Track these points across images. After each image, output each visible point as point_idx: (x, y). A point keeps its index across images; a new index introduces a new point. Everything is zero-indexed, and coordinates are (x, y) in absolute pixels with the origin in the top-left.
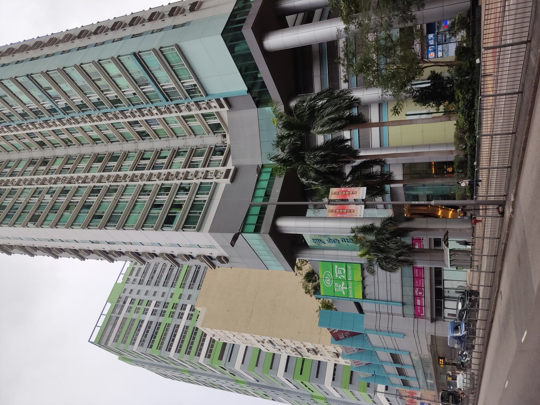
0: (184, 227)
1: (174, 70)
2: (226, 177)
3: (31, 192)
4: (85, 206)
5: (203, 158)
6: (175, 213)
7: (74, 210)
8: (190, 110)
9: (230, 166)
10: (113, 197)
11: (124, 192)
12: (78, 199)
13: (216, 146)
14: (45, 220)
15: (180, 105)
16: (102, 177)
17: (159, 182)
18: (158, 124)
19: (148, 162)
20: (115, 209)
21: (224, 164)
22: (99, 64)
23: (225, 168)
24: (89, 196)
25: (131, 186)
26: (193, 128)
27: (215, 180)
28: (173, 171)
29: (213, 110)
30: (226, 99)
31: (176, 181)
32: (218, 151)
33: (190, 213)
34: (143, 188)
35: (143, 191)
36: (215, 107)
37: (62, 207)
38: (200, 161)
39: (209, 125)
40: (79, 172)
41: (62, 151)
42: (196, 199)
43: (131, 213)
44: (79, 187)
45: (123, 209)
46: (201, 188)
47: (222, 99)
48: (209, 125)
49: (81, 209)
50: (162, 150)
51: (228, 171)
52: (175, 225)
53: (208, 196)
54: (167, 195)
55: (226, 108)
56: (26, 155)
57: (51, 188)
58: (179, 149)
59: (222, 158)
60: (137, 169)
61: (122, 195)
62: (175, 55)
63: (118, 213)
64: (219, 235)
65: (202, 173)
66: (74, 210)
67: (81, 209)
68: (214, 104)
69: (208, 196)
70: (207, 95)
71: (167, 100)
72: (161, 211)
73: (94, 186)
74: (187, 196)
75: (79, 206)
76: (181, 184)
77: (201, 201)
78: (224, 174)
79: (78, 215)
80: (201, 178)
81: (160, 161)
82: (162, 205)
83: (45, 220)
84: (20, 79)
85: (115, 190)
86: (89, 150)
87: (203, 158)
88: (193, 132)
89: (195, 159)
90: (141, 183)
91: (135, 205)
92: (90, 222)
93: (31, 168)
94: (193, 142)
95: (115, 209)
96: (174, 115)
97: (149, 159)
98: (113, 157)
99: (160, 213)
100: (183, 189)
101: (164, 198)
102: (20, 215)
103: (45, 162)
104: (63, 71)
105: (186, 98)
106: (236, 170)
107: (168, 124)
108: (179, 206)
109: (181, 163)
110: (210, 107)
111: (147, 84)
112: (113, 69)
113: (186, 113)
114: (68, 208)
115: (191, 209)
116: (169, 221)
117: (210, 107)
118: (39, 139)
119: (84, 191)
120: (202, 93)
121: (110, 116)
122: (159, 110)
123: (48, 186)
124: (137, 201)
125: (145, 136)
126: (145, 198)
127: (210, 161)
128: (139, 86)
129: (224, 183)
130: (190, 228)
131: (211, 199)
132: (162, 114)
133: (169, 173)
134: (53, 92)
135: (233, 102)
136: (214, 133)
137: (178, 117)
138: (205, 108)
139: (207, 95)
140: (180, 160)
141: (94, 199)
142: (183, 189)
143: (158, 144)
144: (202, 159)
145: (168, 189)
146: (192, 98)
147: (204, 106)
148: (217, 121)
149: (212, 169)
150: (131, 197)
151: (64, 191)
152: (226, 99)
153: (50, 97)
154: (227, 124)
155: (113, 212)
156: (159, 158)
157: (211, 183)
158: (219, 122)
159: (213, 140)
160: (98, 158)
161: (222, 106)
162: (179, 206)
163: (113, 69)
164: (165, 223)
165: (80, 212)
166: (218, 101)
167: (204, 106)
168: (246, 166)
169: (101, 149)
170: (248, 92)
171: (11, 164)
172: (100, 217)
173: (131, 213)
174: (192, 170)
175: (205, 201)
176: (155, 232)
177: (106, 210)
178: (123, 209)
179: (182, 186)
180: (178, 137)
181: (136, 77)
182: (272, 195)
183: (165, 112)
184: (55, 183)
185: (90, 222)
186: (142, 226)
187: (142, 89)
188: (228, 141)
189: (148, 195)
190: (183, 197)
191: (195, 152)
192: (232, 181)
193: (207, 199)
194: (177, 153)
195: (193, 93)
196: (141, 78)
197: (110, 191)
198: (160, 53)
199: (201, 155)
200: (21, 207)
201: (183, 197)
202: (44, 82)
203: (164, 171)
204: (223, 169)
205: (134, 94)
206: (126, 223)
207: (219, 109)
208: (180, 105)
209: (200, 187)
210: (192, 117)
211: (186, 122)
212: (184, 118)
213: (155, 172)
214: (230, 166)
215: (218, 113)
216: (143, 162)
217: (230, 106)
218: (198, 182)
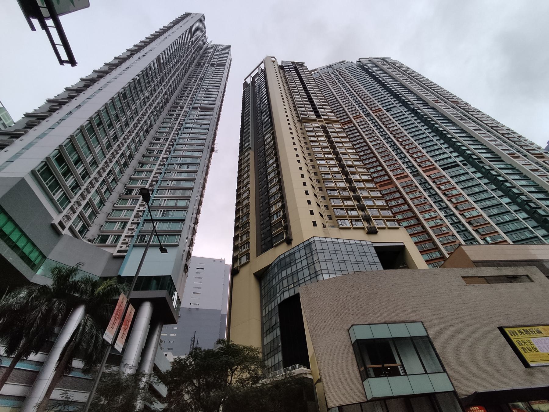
0: (46, 164)
1: (163, 235)
2: (60, 223)
3: (139, 110)
4: (111, 125)
5: (87, 217)
6: (63, 168)
7: (113, 118)
8: (129, 229)
9: (66, 232)
10: (104, 143)
11: (103, 152)
12: (118, 126)
13: (88, 230)
14: (120, 99)
15: (136, 225)
16: (120, 149)
17: (92, 176)
18: (131, 204)
19: (110, 180)
20: (96, 137)
21: (71, 229)
22: (188, 199)
23: (67, 227)
24: (115, 133)
25: (103, 159)
26: (113, 224)
27: (65, 212)
28: (93, 191)
29: (119, 244)
30: (123, 257)
31: (83, 188)
32: (85, 229)
33: (54, 177)
34: (96, 164)
35: (95, 163)
36: (121, 247)
37: (120, 115)
38: (86, 212)
39: (109, 235)
40: (131, 142)
41: (146, 144)
42: (61, 190)
43: (87, 143)
44: (123, 133)
45: (92, 140)
46: (66, 199)
47: (125, 254)
48: (109, 235)
49: (111, 121)
50: (111, 194)
51: (63, 227)
52: (53, 160)
53: (56, 200)
54: (80, 174)
55: (115, 254)
56: (155, 127)
57: (133, 121)
58: (104, 205)
59: (77, 229)
60: (110, 171)
61: (101, 149)
62: (173, 241)
63: (93, 136)
64: (15, 183)
65: (77, 208)
66: (113, 118)
67: (111, 121)
68: (124, 247)
69: (56, 200)
70: (134, 246)
71: (145, 220)
72: (72, 160)
73: (118, 141)
74: (68, 186)
75: (114, 123)
76: (80, 189)
77: (56, 192)
78: (64, 223)
79: (109, 116)
80: (74, 205)
81: (105, 188)
82: (76, 165)
83: (120, 99)
84: (199, 160)
85: (107, 148)
86: (138, 156)
87: (87, 217)
88: (110, 221)
89: (90, 210)
90: (100, 166)
91: (89, 149)
92: (99, 117)
93: (149, 123)
94: (101, 218)
95: (96, 137)
96: (132, 218)
97: (111, 182)
98: (126, 165)
99: (72, 158)
100: (76, 187)
101: (80, 170)
102: (131, 93)
103: (147, 132)
104: (193, 180)
105: (140, 232)
106: (59, 234)
107: (128, 210)
108: (65, 174)
109: (94, 200)
110: (123, 243)
111: (163, 215)
112: (182, 204)
113: (128, 226)
114: (117, 116)
115: (56, 180)
116: (60, 159)
117: (123, 243)
118: (162, 140)
119: (119, 133)
120: (137, 244)
121: (154, 183)
122: (141, 211)
123: (135, 120)
124: (91, 153)
125: (127, 192)
126: (89, 159)
127: (81, 220)
128: (164, 211)
129: (56, 219)
130: (42, 168)
131: (51, 200)
132: (137, 211)
133: (94, 187)
134: (185, 168)
135: (118, 261)
136: (99, 236)
137: (129, 219)
138: (124, 240)
139: (134, 246)
140: (96, 201)
141: (112, 133)
142: (76, 187)
143: (114, 197)
144: (87, 215)
145: (84, 177)
146: (138, 236)
147: (127, 240)
148: (109, 242)
149: (74, 217)
150: (97, 152)
151: (127, 124)
152: (123, 257)
153: (184, 164)
154: (102, 248)
155: (95, 134)
156: (107, 189)
157: (64, 209)
158: (107, 244)
159: (93, 232)
160: (131, 157)
161: (119, 251)
162: (65, 174)
163: (182, 204)
164: (61, 155)
165: (110, 119)
166: (125, 251)
167: (127, 240)
168: (55, 244)
169: (134, 163)
170: (120, 276)
171: (156, 118)
172: (98, 125)
173: (87, 143)
174: (84, 203)
175: (54, 194)
176: (60, 144)
177: (99, 132)
178: (92, 140)
179: (78, 188)
180: (113, 210)
181: (171, 213)
182: (11, 252)
183: (137, 214)
184: (134, 125)
185: (99, 117)
186: (71, 139)
187: (161, 211)
188: (85, 241)
189: (90, 163)
190: (70, 182)
191: (94, 214)
192: (53, 226)
193: (54, 197)
194: (102, 202)
195: (141, 238)
196: (168, 215)
197: (109, 146)
198: (178, 233)
199: (90, 217)
200: (135, 99)
201: (70, 182)
202: (192, 168)
203: (97, 185)
204: (68, 225)
205: (160, 204)
206: (82, 134)
207: (118, 248)
208: (136, 225)
209: (68, 199)
210: (123, 228)
211: (122, 222)
212: (126, 223)
213: (101, 180)
214: (66, 232)
215: (116, 246)
216: (112, 178)
217: (115, 257)
218: (73, 201)
